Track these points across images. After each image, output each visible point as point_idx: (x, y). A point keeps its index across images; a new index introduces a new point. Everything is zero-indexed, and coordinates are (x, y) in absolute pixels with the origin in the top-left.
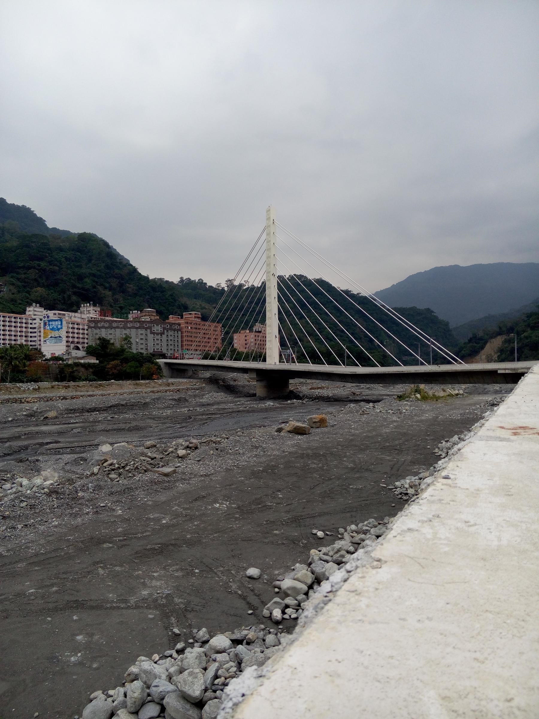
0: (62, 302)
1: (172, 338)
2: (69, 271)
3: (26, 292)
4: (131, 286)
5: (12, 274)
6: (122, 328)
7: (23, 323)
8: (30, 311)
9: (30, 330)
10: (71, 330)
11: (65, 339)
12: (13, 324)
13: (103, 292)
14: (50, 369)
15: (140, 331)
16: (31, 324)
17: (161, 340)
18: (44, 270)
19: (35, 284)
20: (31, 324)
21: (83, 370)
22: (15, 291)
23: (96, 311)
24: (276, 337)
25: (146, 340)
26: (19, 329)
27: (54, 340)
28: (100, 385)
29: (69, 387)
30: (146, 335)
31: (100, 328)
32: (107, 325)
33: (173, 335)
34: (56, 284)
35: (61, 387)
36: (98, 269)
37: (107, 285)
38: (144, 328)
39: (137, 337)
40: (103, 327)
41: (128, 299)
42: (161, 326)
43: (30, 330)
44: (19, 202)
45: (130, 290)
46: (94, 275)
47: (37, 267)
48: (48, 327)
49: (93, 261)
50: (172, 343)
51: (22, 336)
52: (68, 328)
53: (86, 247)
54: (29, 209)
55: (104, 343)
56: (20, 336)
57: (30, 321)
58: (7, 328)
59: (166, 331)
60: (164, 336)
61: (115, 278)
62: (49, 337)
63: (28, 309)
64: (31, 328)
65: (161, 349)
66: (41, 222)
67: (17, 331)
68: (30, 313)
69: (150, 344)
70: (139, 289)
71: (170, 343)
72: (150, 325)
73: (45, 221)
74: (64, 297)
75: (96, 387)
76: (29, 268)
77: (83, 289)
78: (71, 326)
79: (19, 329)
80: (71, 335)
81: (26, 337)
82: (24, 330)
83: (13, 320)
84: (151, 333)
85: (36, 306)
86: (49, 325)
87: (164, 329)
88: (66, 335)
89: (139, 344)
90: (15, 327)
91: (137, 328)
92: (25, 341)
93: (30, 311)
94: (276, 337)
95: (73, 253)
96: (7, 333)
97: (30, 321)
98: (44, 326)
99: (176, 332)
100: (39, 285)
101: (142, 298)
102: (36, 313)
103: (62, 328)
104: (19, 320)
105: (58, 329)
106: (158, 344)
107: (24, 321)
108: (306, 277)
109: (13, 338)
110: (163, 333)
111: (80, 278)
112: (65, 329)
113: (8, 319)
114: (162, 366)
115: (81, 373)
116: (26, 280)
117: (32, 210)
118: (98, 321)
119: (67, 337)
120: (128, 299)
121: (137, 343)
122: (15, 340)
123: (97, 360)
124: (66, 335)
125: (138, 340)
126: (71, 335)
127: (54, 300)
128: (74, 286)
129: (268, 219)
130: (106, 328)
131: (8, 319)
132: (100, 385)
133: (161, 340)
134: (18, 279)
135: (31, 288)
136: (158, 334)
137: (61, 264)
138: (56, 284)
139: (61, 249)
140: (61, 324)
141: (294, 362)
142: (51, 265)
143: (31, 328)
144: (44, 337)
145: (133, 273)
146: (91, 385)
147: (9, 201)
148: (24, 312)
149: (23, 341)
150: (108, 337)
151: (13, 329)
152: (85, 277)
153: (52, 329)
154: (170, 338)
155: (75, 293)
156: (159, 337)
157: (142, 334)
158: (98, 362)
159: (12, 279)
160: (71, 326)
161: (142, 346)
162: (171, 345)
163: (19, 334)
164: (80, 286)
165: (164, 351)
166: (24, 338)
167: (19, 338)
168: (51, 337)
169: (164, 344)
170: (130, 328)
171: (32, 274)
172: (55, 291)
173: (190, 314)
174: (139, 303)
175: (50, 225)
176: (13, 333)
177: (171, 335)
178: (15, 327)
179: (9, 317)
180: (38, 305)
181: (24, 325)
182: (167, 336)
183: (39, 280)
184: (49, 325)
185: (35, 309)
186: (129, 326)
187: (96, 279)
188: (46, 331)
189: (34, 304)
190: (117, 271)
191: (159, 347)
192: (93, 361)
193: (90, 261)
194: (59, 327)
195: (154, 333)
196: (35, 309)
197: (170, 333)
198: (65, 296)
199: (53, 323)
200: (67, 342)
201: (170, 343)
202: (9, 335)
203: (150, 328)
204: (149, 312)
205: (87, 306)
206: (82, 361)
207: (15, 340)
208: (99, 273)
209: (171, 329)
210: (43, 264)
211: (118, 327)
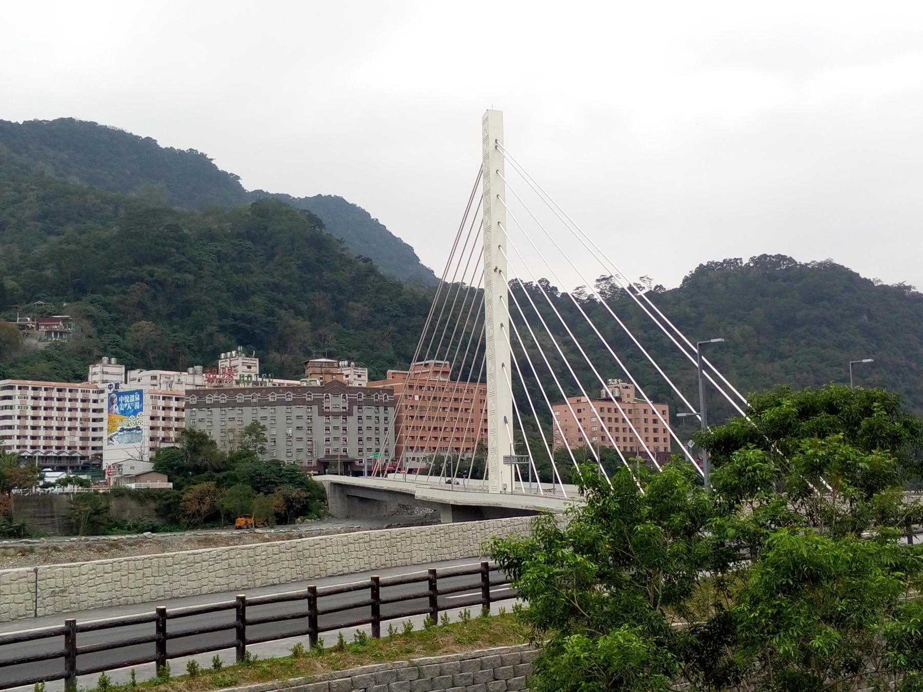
0: (196, 348)
1: (371, 423)
2: (216, 283)
3: (118, 333)
4: (359, 305)
5: (95, 296)
6: (255, 405)
7: (76, 400)
8: (95, 374)
9: (92, 415)
10: (161, 413)
11: (147, 433)
12: (55, 404)
13: (293, 322)
14: (55, 506)
15: (296, 411)
16: (95, 401)
17: (345, 429)
18: (162, 284)
19: (139, 314)
20: (95, 401)
21: (133, 504)
22: (92, 331)
23: (249, 367)
24: (506, 421)
25: (310, 429)
26: (67, 414)
27: (127, 436)
28: (114, 545)
29: (32, 551)
30: (310, 418)
31: (208, 407)
32: (291, 397)
33: (373, 416)
34: (185, 311)
35: (12, 551)
36: (285, 273)
37: (303, 307)
38: (304, 402)
39: (289, 425)
40: (216, 405)
41: (349, 335)
42: (344, 397)
43: (92, 415)
44: (183, 145)
45: (355, 314)
46: (276, 287)
47: (149, 278)
48: (116, 409)
49: (277, 258)
50: (371, 434)
51: (76, 428)
52: (154, 408)
53: (265, 229)
54: (203, 156)
55: (197, 441)
56: (70, 429)
57: (93, 396)
58: (42, 413)
59: (355, 408)
60: (352, 421)
61: (325, 289)
62: (118, 429)
63: (92, 369)
64: (94, 411)
65: (345, 451)
66: (229, 182)
67: (63, 419)
68: (95, 378)
69: (320, 436)
70: (377, 311)
71: (366, 434)
72: (318, 395)
73: (238, 178)
74: (199, 338)
75: (100, 550)
76: (131, 280)
77: (243, 318)
78: (161, 403)
79: (67, 414)
80: (160, 423)
81: (83, 429)
82: (79, 414)
83: (55, 394)
84: (322, 413)
85: (109, 362)
86: (119, 403)
87: (352, 402)
88: (150, 423)
89: (294, 440)
90: (59, 409)
91: (288, 404)
92: (82, 439)
93: (95, 374)
94: (506, 421)
95: (236, 242)
96: (42, 423)
97: (93, 396)
98: (109, 407)
99: (382, 409)
100: (146, 315)
101: (379, 332)
102: (106, 377)
103: (141, 409)
104: (68, 395)
105: (135, 412)
106: (336, 439)
107: (79, 396)
108: (791, 260)
109: (55, 433)
110: (350, 413)
111: (241, 295)
112: (148, 411)
113: (43, 394)
114: (328, 491)
115: (128, 511)
116: (120, 307)
117: (209, 157)
118: (206, 392)
119: (152, 428)
120: (349, 335)
121: (289, 437)
122: (59, 438)
123: (169, 481)
124: (150, 423)
125: (290, 431)
126: (160, 423)
127: (177, 345)
128: (223, 314)
129: (486, 140)
130: (222, 406)
131: (43, 394)
132: (114, 545)
133: (345, 429)
134: (105, 306)
135: (129, 325)
136: (336, 415)
137: (201, 269)
138: (185, 311)
139: (211, 236)
140: (141, 401)
141: (536, 481)
142: (179, 271)
143: (94, 411)
144: (109, 430)
145: (367, 276)
146: (89, 546)
147: (163, 144)
148: (82, 377)
149: (77, 439)
150: (201, 427)
151: (55, 413)
152: (254, 293)
153: (124, 413)
154: (366, 423)
155: (223, 329)
156: (339, 422)
157: (299, 417)
158: (171, 485)
159: (90, 307)
160: (161, 403)
161: (301, 445)
162: (369, 439)
163: (67, 424)
164: (238, 311)
165: (353, 454)
166: (79, 433)
167: (66, 433)
168: (122, 430)
169: (353, 437)
170: (272, 404)
171: (137, 292)
172: (182, 327)
173: (426, 365)
174: (370, 343)
175: (249, 185)
176: (54, 423)
177: (369, 417)
178: (59, 409)
179: (46, 389)
180: (113, 360)
181: (79, 405)
182: (360, 418)
183: (149, 303)
184: (119, 403)
185: (106, 369)
186: (271, 400)
187: (280, 296)
188: (113, 416)
189: (105, 359)
190: (327, 275)
191: (338, 445)
192: (162, 483)
193: (270, 257)
194: (137, 407)
195: (327, 415)
196: (106, 369)
197: (367, 411)
198: (203, 335)
199: (126, 398)
200: (152, 439)
201: (366, 434)
202: (46, 428)
203: (319, 402)
204: (321, 365)
205: (231, 356)
206: (133, 486)
207: (59, 438)
208: (286, 282)
209: (369, 403)
210: (160, 271)
211: (247, 404)
